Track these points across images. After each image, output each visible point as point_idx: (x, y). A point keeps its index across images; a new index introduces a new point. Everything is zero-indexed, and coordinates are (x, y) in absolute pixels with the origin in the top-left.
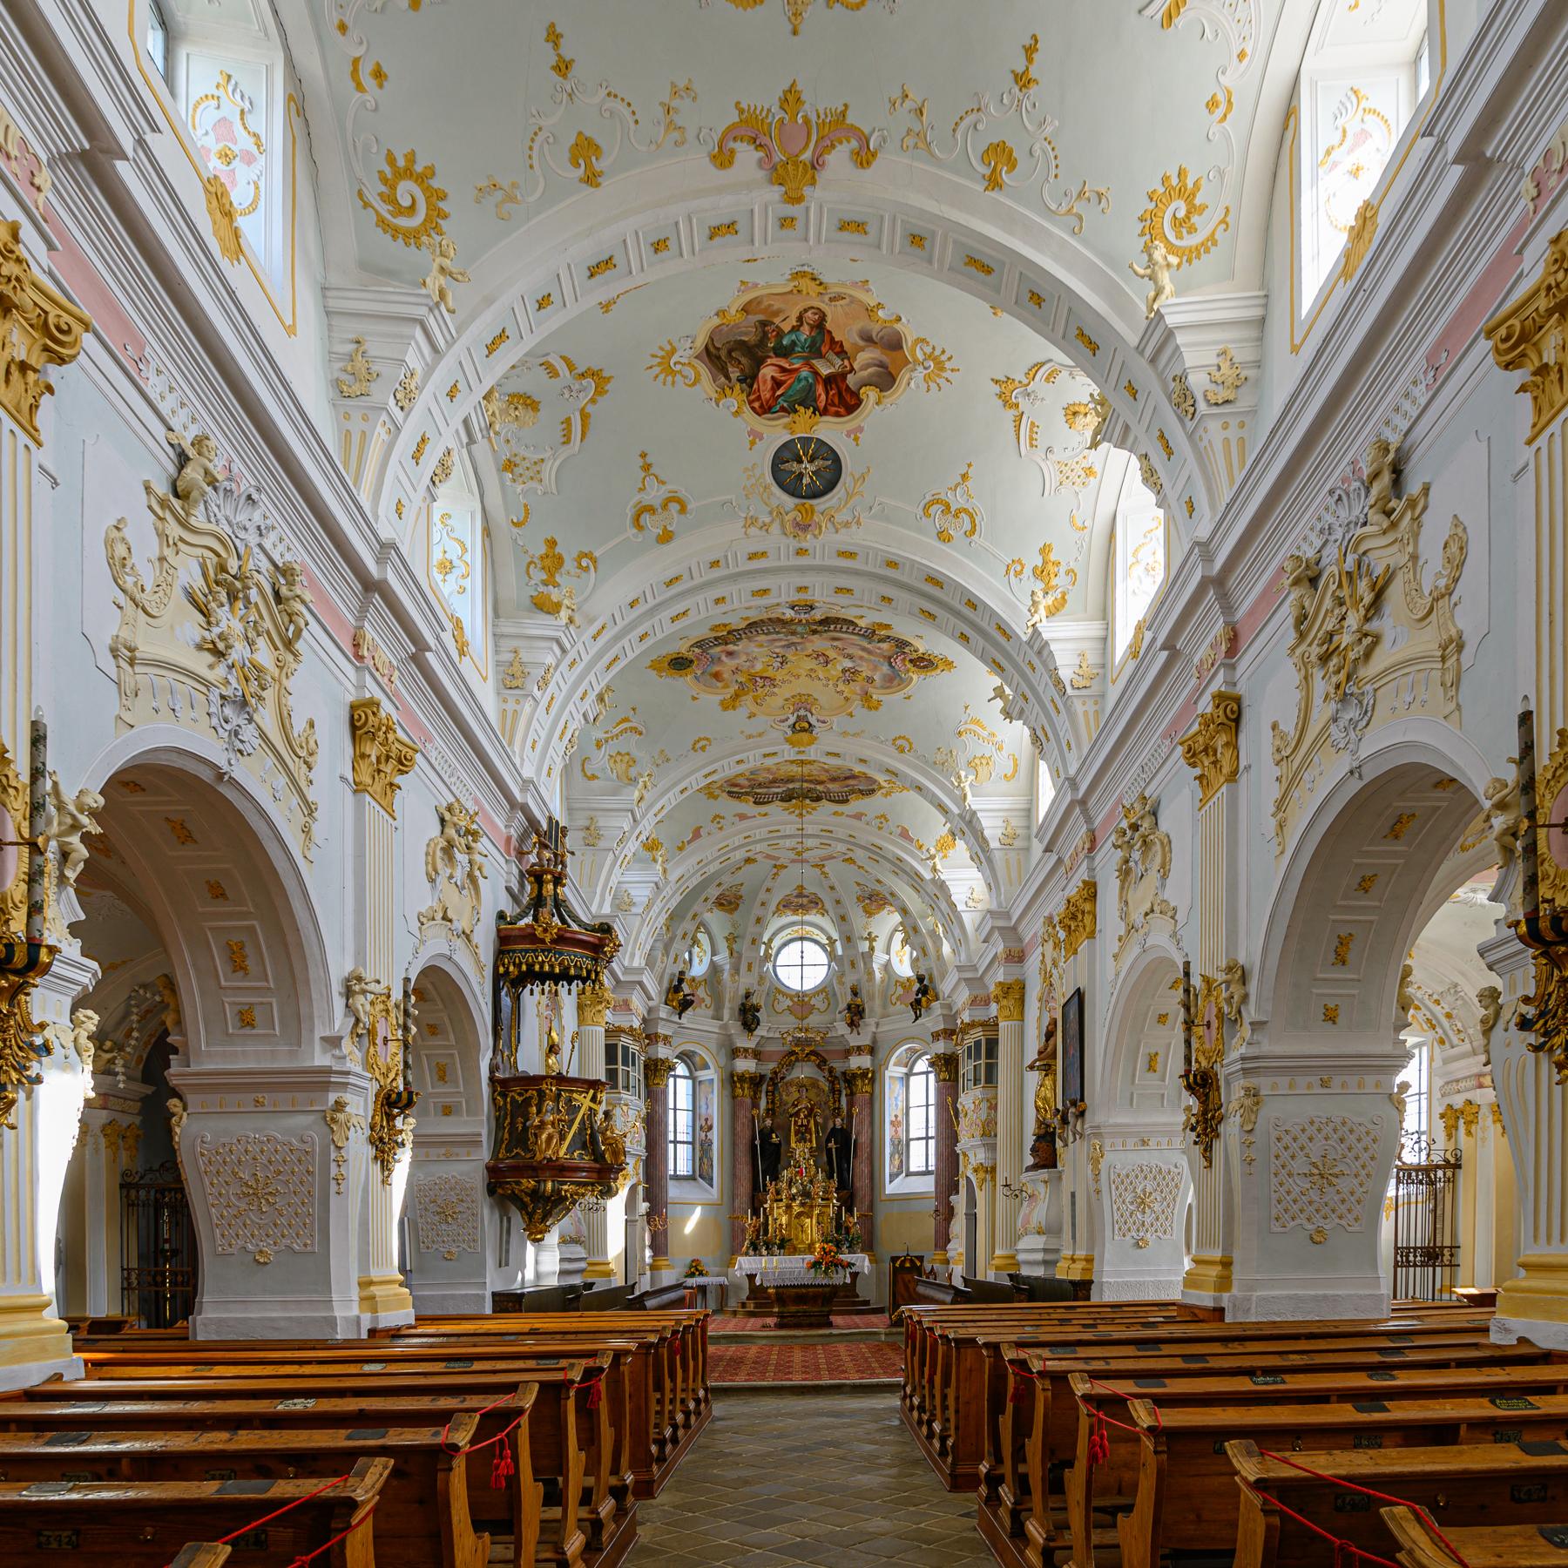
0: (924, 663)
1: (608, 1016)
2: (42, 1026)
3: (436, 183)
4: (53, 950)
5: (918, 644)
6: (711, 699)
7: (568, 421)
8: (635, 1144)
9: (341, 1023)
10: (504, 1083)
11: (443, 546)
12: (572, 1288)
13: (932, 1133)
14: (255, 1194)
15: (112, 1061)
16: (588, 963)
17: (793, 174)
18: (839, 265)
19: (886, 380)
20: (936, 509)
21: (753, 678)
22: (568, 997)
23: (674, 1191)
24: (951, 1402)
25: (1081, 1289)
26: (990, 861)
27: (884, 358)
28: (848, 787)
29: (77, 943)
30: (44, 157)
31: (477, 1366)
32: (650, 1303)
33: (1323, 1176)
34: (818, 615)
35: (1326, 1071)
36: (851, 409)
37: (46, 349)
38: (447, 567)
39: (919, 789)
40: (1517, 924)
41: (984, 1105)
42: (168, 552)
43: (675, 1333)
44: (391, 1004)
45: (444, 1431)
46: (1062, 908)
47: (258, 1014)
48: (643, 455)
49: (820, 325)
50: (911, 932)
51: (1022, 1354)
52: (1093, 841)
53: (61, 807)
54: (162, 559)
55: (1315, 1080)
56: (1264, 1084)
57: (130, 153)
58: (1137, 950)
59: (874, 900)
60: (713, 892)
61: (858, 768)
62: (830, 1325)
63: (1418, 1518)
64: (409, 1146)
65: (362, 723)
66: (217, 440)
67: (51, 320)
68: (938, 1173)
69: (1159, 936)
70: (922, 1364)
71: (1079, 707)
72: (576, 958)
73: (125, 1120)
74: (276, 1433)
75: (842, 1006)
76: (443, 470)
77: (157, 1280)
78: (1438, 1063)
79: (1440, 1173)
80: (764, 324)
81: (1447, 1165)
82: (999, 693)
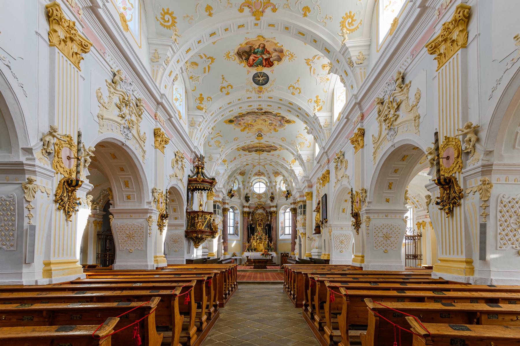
0: (288, 122)
1: (214, 198)
2: (79, 199)
3: (174, 15)
4: (82, 182)
5: (286, 117)
6: (238, 129)
7: (205, 68)
8: (220, 227)
9: (151, 199)
10: (189, 213)
11: (176, 95)
12: (205, 259)
13: (291, 225)
14: (129, 237)
15: (96, 207)
16: (210, 186)
17: (258, 14)
18: (268, 34)
19: (279, 59)
20: (291, 88)
21: (248, 125)
22: (205, 194)
23: (229, 237)
24: (296, 287)
25: (327, 261)
26: (304, 165)
27: (279, 55)
28: (270, 149)
29: (88, 180)
30: (81, 7)
31: (182, 276)
32: (223, 262)
33: (387, 237)
34: (263, 111)
35: (386, 213)
36: (271, 66)
37: (82, 50)
38: (177, 100)
39: (287, 149)
40: (435, 180)
41: (303, 219)
42: (111, 95)
43: (229, 269)
44: (163, 195)
45: (173, 291)
46: (322, 175)
47: (131, 196)
48: (223, 76)
49: (264, 47)
50: (285, 181)
51: (313, 276)
52: (329, 161)
53: (85, 150)
54: (110, 97)
55: (384, 215)
56: (371, 216)
57: (102, 7)
58: (339, 185)
59: (277, 174)
60: (239, 171)
61: (273, 145)
62: (266, 268)
63: (416, 320)
64: (167, 226)
65: (156, 133)
66: (123, 71)
67: (83, 44)
68: (292, 234)
69: (345, 182)
70: (289, 278)
71: (325, 131)
72: (206, 185)
73: (99, 220)
74: (132, 291)
75: (269, 197)
76: (176, 78)
77: (105, 256)
78: (415, 212)
79: (416, 238)
80: (251, 47)
81: (418, 235)
82: (306, 128)
